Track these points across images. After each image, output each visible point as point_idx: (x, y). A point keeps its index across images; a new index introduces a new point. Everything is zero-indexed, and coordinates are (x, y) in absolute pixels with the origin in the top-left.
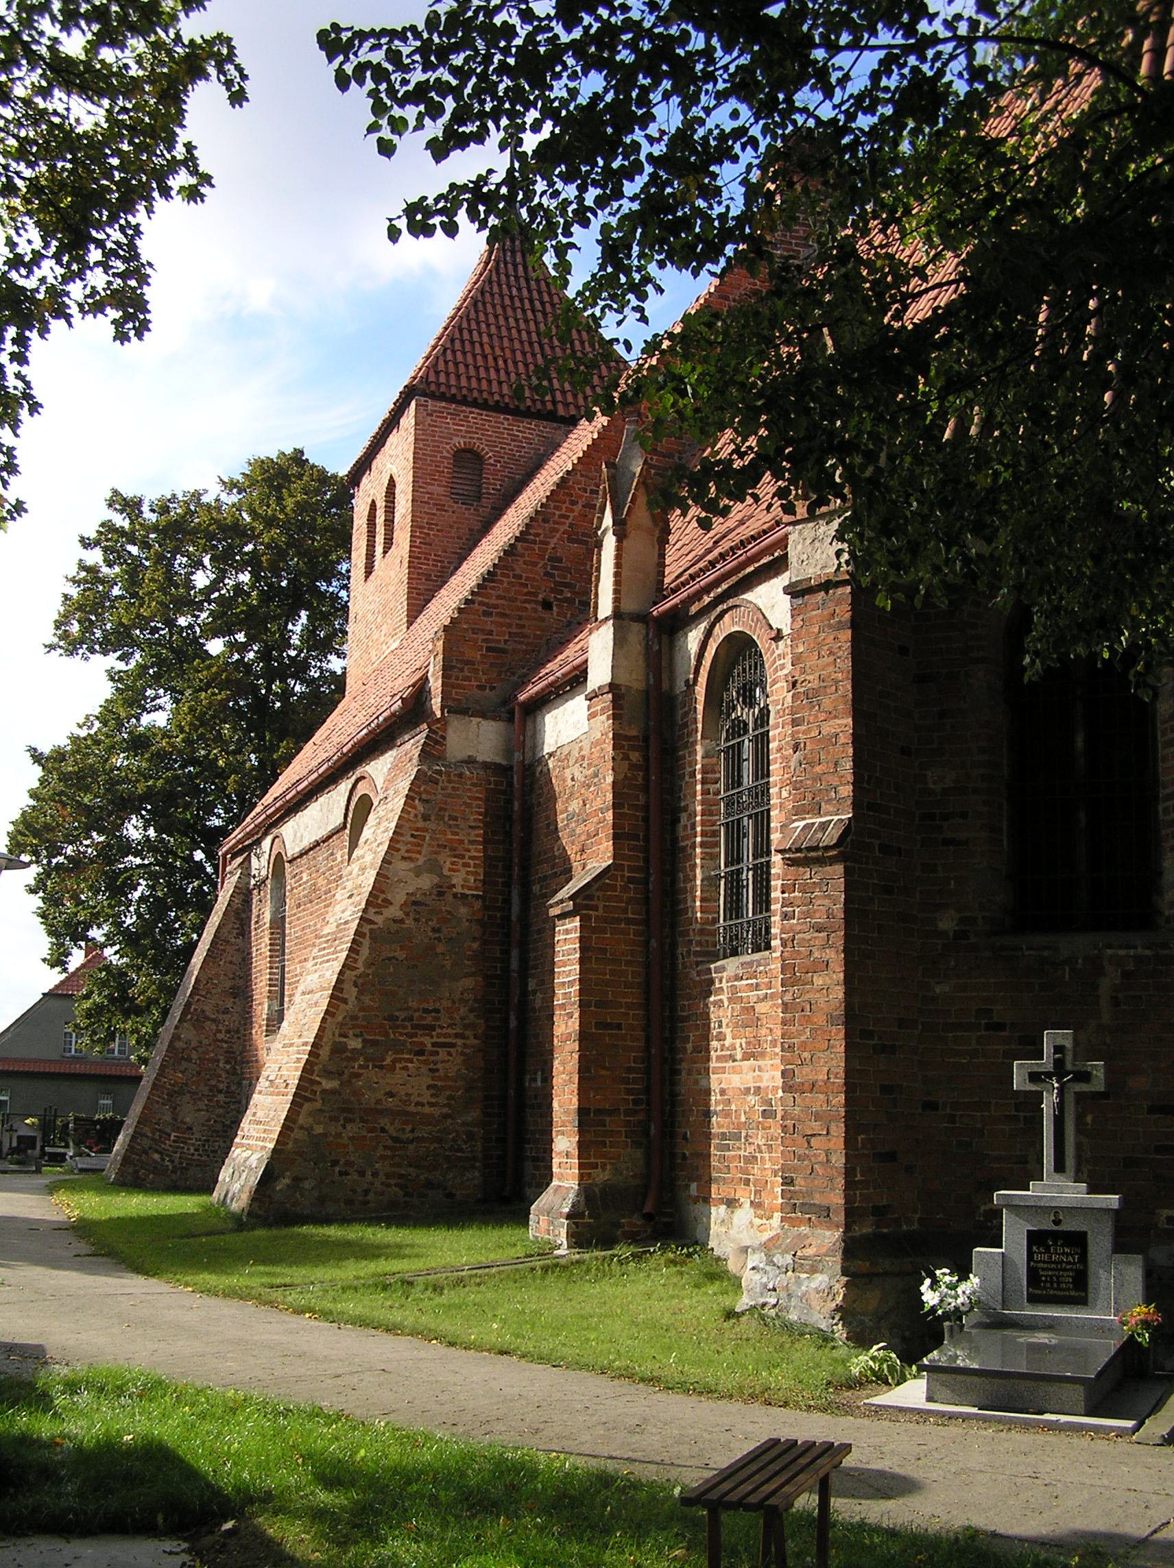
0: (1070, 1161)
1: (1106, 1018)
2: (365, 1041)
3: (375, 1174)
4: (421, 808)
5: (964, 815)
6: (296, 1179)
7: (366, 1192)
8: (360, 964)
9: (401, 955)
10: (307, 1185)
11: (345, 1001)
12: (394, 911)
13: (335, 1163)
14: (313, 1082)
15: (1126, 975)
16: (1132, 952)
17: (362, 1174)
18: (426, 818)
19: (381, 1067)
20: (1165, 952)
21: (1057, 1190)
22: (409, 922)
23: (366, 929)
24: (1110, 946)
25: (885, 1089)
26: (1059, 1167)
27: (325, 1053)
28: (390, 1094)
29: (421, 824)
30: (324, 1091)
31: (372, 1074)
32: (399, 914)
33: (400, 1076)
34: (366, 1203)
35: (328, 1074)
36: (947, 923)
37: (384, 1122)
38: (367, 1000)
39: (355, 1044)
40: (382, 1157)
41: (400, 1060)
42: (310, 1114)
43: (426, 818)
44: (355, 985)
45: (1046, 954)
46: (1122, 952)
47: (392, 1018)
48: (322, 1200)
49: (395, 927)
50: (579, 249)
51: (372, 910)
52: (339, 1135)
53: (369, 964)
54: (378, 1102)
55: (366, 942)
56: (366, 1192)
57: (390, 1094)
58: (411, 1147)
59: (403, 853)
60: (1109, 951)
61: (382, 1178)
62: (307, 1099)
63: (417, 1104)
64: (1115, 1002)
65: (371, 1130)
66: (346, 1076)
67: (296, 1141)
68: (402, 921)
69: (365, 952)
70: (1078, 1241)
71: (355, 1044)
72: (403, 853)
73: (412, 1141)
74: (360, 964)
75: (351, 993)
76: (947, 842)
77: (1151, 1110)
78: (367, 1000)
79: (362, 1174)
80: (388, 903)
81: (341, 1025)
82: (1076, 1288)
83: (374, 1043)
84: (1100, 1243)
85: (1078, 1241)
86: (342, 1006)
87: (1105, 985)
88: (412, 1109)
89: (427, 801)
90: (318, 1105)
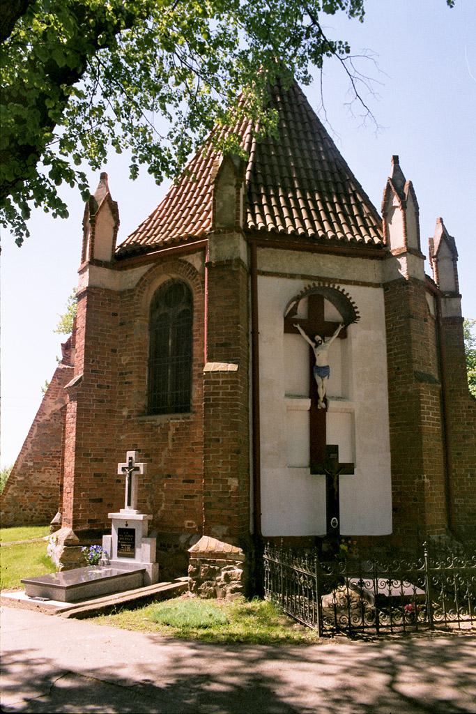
0: (133, 502)
1: (170, 447)
2: (34, 463)
3: (36, 510)
4: (58, 381)
5: (131, 373)
6: (6, 512)
7: (32, 517)
8: (33, 436)
9: (48, 432)
10: (10, 514)
11: (27, 449)
12: (47, 417)
13: (21, 506)
14: (14, 478)
15: (177, 429)
16: (179, 421)
17: (31, 510)
18: (59, 384)
19: (40, 472)
20: (188, 421)
21: (129, 514)
22: (52, 421)
23: (36, 423)
24: (172, 419)
25: (96, 475)
26: (129, 505)
27: (19, 467)
28: (43, 481)
29: (57, 386)
30: (18, 481)
31: (36, 474)
32: (49, 418)
33: (47, 474)
34: (32, 520)
35: (19, 475)
36: (125, 413)
37: (40, 491)
38: (35, 448)
39: (31, 464)
40: (40, 504)
41: (47, 469)
42: (13, 489)
43: (59, 384)
44: (31, 443)
45: (153, 423)
46: (176, 421)
47: (44, 454)
48: (15, 520)
49: (46, 423)
50: (396, 159)
51: (38, 417)
52: (23, 496)
53: (37, 436)
54: (39, 484)
55: (36, 428)
56: (32, 517)
57: (43, 481)
58: (50, 500)
59: (51, 396)
60: (172, 421)
61: (39, 511)
62: (12, 484)
63: (53, 485)
64: (173, 440)
65: (35, 494)
66: (26, 476)
67: (7, 499)
68: (49, 420)
69: (35, 431)
70: (132, 532)
71: (31, 464)
72: (51, 396)
73: (50, 498)
74: (33, 436)
75: (30, 446)
76: (126, 383)
77: (184, 481)
78: (35, 448)
79: (31, 510)
80: (44, 414)
81: (26, 457)
82: (132, 551)
83: (38, 463)
84: (138, 535)
85: (132, 532)
86: (26, 451)
87: (170, 433)
88: (51, 486)
89: (60, 378)
90: (16, 486)
